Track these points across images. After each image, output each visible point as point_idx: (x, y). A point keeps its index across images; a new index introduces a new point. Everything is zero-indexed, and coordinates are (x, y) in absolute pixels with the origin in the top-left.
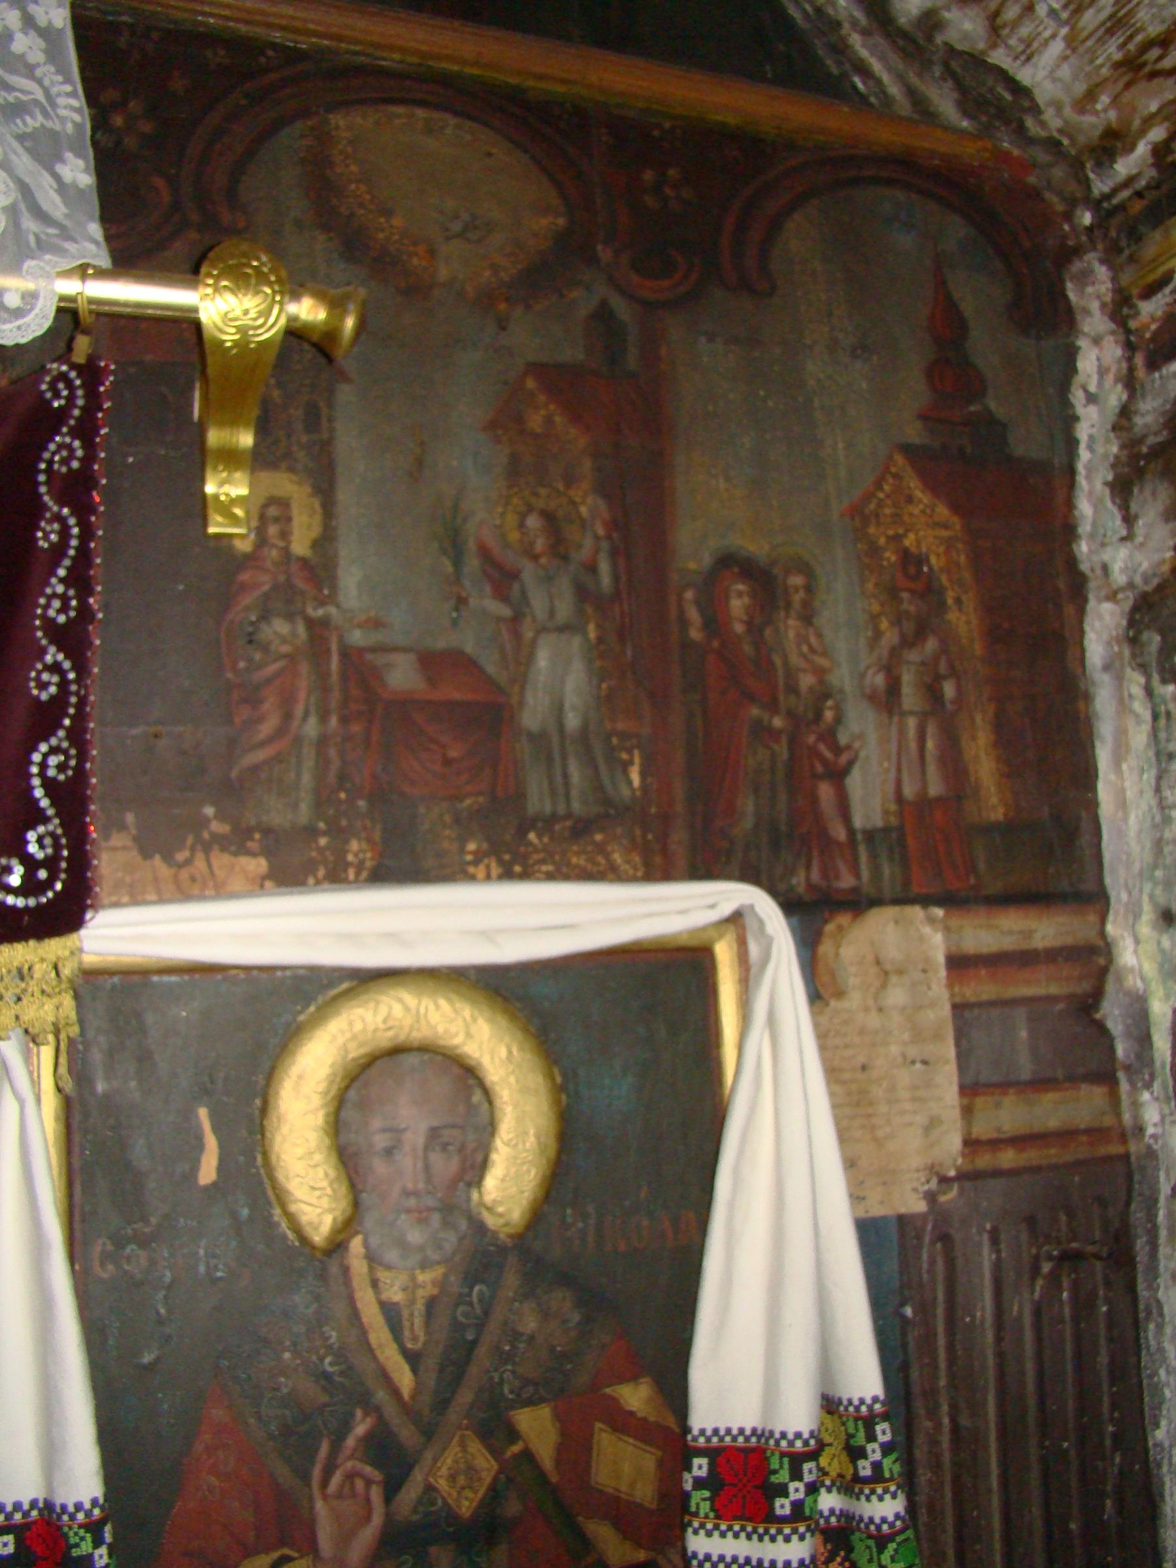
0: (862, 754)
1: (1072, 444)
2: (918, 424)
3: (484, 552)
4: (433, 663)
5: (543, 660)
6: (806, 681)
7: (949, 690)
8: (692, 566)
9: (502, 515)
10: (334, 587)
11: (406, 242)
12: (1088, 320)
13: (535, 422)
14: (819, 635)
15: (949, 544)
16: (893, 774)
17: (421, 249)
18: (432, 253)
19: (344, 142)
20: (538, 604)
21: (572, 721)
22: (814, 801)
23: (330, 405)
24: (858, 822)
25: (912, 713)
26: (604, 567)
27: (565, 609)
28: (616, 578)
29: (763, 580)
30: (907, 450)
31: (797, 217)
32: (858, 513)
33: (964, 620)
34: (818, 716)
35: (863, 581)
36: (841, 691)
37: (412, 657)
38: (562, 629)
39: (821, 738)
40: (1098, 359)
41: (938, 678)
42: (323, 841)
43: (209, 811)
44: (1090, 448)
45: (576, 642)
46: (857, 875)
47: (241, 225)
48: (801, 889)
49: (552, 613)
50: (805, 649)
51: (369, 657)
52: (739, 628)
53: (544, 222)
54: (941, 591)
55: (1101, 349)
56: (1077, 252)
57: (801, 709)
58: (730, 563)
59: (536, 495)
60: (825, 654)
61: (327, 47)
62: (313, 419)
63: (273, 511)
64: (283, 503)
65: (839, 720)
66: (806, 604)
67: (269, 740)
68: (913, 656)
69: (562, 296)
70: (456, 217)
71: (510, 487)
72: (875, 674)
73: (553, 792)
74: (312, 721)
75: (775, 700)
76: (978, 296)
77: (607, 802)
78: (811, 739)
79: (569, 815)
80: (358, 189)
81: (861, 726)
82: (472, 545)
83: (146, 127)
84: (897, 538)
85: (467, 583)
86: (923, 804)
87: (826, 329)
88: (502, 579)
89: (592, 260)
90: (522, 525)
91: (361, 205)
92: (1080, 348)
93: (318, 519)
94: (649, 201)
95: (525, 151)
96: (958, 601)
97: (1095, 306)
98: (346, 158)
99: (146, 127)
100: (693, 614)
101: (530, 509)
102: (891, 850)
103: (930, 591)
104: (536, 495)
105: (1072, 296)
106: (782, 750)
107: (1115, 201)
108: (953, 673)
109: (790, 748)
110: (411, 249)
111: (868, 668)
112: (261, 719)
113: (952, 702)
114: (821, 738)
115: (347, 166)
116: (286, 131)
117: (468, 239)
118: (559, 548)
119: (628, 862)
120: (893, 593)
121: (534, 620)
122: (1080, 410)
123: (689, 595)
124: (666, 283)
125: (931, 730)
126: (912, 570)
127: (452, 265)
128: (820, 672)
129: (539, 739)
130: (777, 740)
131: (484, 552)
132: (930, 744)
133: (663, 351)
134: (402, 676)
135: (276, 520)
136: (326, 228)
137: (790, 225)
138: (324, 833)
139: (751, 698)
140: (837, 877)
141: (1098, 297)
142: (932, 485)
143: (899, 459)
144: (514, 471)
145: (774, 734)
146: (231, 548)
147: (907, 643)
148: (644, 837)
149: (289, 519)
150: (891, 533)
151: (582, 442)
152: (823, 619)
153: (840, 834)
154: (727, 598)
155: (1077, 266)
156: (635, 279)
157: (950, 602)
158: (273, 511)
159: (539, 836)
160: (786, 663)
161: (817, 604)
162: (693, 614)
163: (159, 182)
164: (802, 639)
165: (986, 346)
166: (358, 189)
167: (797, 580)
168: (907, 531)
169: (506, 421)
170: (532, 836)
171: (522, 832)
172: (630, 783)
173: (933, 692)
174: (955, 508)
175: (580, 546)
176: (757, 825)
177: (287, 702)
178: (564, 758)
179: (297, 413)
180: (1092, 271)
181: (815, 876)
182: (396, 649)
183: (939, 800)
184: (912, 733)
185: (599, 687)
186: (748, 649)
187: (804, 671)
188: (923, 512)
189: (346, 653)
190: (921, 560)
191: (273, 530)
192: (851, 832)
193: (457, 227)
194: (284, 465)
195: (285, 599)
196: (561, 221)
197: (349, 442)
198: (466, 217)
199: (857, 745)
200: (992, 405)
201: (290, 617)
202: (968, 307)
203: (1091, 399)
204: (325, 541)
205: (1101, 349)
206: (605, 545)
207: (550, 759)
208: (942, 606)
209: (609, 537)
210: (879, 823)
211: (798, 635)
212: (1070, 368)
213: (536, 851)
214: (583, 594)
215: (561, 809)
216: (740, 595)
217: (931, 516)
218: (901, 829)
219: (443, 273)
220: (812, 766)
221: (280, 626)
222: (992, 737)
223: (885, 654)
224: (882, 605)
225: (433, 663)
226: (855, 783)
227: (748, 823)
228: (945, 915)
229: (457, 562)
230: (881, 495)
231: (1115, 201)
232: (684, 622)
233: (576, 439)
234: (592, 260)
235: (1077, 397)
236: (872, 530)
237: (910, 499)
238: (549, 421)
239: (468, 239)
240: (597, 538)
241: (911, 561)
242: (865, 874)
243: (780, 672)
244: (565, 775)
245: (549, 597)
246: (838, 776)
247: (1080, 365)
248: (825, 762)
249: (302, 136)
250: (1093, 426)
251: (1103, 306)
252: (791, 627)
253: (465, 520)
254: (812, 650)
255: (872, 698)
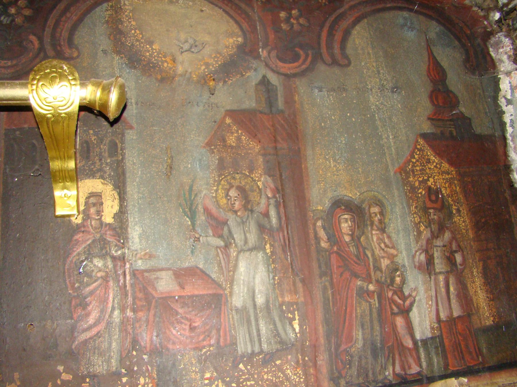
0: (417, 298)
1: (503, 125)
2: (429, 123)
3: (206, 210)
4: (182, 275)
5: (242, 267)
6: (385, 263)
7: (458, 258)
8: (320, 208)
9: (216, 191)
10: (126, 239)
11: (160, 56)
12: (502, 65)
13: (232, 140)
14: (389, 237)
15: (450, 182)
16: (434, 307)
17: (168, 59)
18: (174, 60)
19: (128, 11)
20: (238, 236)
21: (260, 300)
22: (394, 327)
23: (123, 142)
24: (418, 336)
25: (440, 273)
26: (273, 213)
27: (253, 238)
28: (279, 218)
29: (356, 211)
30: (424, 136)
31: (357, 27)
32: (402, 170)
33: (462, 220)
34: (393, 280)
35: (409, 206)
36: (404, 266)
37: (170, 273)
38: (251, 250)
39: (395, 293)
40: (510, 83)
41: (453, 252)
42: (124, 380)
43: (61, 368)
44: (512, 126)
45: (260, 255)
46: (420, 366)
47: (75, 55)
48: (390, 378)
49: (246, 242)
50: (383, 245)
51: (146, 274)
52: (347, 239)
53: (231, 40)
54: (449, 207)
55: (511, 78)
56: (492, 34)
57: (383, 279)
58: (340, 205)
59: (234, 178)
60: (393, 247)
61: (399, 303)
62: (114, 149)
63: (92, 200)
64: (98, 195)
65: (403, 281)
66: (381, 222)
67: (95, 325)
68: (439, 242)
69: (243, 76)
70: (186, 41)
71: (219, 176)
72: (420, 254)
73: (251, 341)
74: (116, 313)
75: (369, 275)
76: (449, 58)
77: (282, 342)
78: (390, 294)
79: (261, 352)
80: (135, 32)
81: (416, 284)
82: (200, 208)
83: (27, 12)
84: (425, 181)
85: (199, 230)
86: (452, 321)
87: (378, 80)
88: (218, 225)
89: (258, 57)
90: (227, 195)
91: (137, 40)
92: (500, 78)
93: (117, 202)
94: (284, 26)
95: (220, 8)
96: (458, 211)
97: (505, 58)
98: (130, 18)
99: (27, 12)
100: (322, 234)
101: (231, 186)
102: (436, 348)
103: (443, 207)
104: (234, 178)
105: (492, 54)
106: (375, 302)
107: (510, 7)
108: (460, 248)
109: (380, 302)
110: (163, 59)
111: (416, 252)
112: (88, 315)
113: (460, 265)
114: (395, 293)
115: (130, 22)
116: (98, 9)
117: (193, 52)
118: (248, 205)
119: (295, 374)
120: (425, 210)
121: (236, 246)
122: (504, 108)
123: (319, 223)
124: (296, 64)
125: (452, 280)
126: (433, 198)
127: (185, 65)
128: (392, 257)
129: (242, 311)
130: (372, 297)
131: (206, 210)
132: (452, 289)
133: (296, 98)
134: (165, 284)
135: (94, 205)
136: (118, 53)
137: (354, 32)
138: (125, 375)
139: (356, 276)
140: (410, 368)
141: (506, 53)
142: (439, 154)
143: (421, 141)
144: (221, 166)
145: (370, 294)
146: (70, 221)
147: (435, 236)
148: (303, 359)
149: (102, 204)
150: (421, 179)
151: (257, 148)
152: (391, 229)
153: (409, 343)
154: (340, 223)
155: (493, 40)
156: (280, 64)
157: (454, 212)
158: (92, 200)
159: (245, 367)
160: (373, 255)
161: (386, 221)
162: (322, 234)
163: (33, 38)
164: (381, 240)
165: (457, 80)
166: (135, 32)
167: (375, 209)
168: (429, 177)
169: (216, 141)
170: (241, 366)
171: (235, 366)
172: (294, 330)
173: (450, 260)
174: (451, 163)
175: (259, 204)
176: (364, 345)
177: (104, 301)
178: (257, 320)
179: (104, 147)
180: (501, 42)
181: (398, 369)
182: (162, 270)
183: (459, 317)
184: (442, 284)
185: (274, 279)
186: (353, 249)
187: (383, 257)
188: (435, 167)
189: (134, 273)
190: (438, 192)
191: (93, 210)
192: (415, 342)
193: (186, 47)
194: (98, 175)
195: (100, 247)
196: (240, 39)
197: (132, 159)
198: (191, 41)
199: (414, 294)
200: (463, 110)
201: (103, 257)
202: (445, 63)
203: (509, 102)
204: (121, 215)
205: (511, 78)
206: (272, 201)
207: (249, 322)
208: (450, 215)
209: (274, 197)
210: (430, 335)
211: (378, 239)
212: (497, 89)
213: (244, 374)
214: (261, 228)
215: (257, 349)
216: (346, 220)
217: (440, 168)
218: (441, 337)
219: (180, 69)
220: (392, 309)
221: (98, 263)
222: (483, 281)
223: (424, 242)
224: (420, 218)
225: (182, 275)
226: (415, 314)
227: (360, 344)
228: (469, 381)
229: (193, 218)
230: (414, 160)
231: (510, 7)
232: (317, 239)
233: (255, 147)
234: (258, 57)
235: (502, 102)
236: (411, 179)
237: (429, 161)
238: (239, 139)
239: (193, 52)
240: (268, 198)
241: (433, 193)
242: (424, 364)
243: (371, 260)
244: (258, 330)
245: (245, 233)
246: (406, 312)
247: (501, 86)
248: (398, 306)
249: (107, 10)
250: (512, 115)
251: (509, 57)
252: (375, 235)
253: (196, 195)
254: (386, 246)
255: (420, 268)
